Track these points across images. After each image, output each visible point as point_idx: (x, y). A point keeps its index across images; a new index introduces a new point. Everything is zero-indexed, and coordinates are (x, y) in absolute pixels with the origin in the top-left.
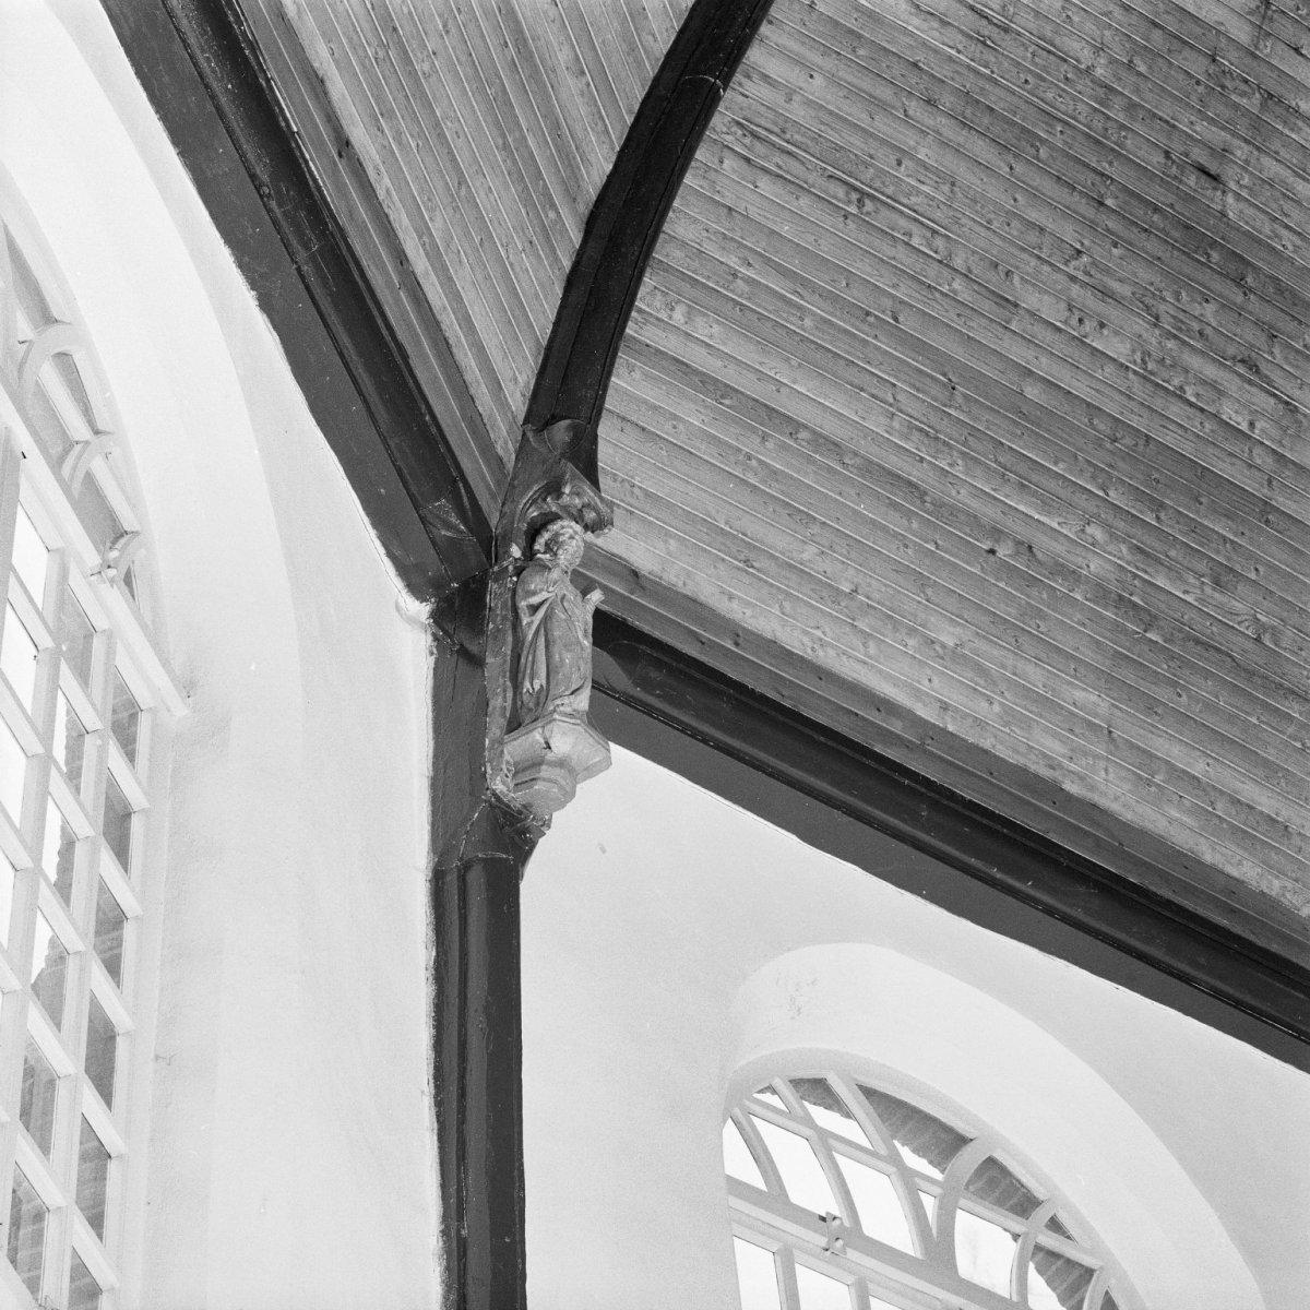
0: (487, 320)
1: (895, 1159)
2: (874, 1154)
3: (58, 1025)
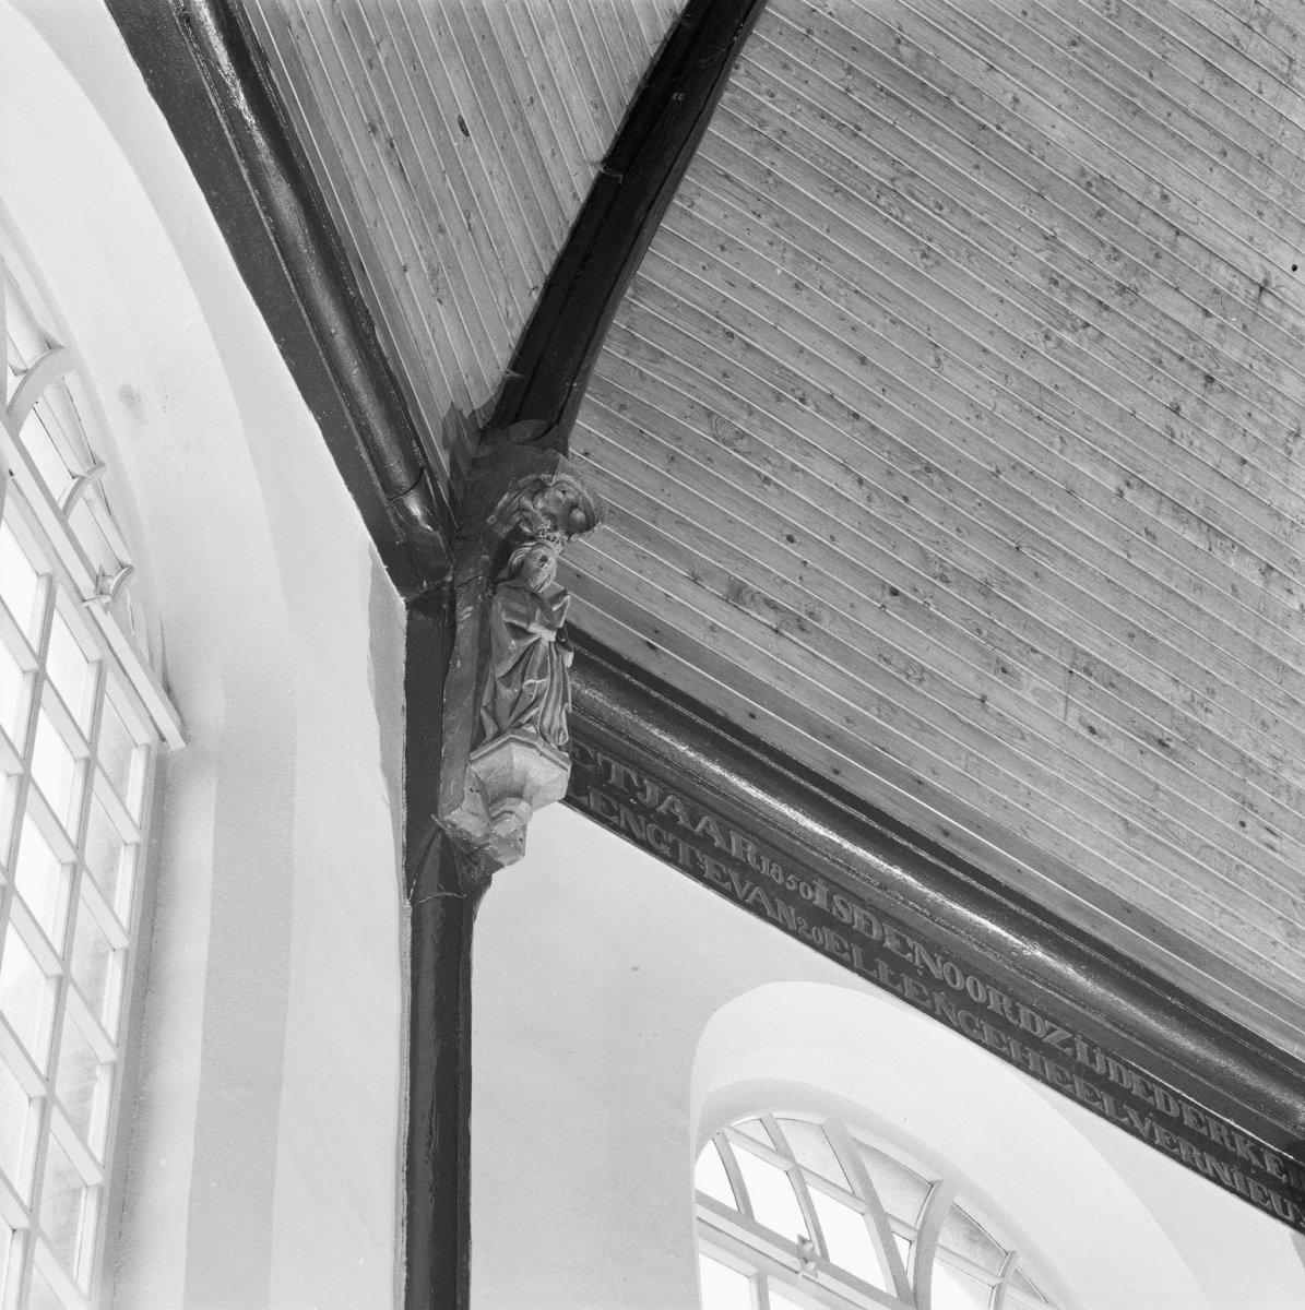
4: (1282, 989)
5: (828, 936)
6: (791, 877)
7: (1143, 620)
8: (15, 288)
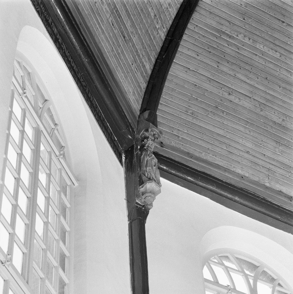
0: (132, 92)
1: (243, 272)
2: (238, 271)
3: (65, 273)
4: (128, 101)
5: (49, 29)
6: (46, 12)
7: (130, 9)
8: (32, 106)
